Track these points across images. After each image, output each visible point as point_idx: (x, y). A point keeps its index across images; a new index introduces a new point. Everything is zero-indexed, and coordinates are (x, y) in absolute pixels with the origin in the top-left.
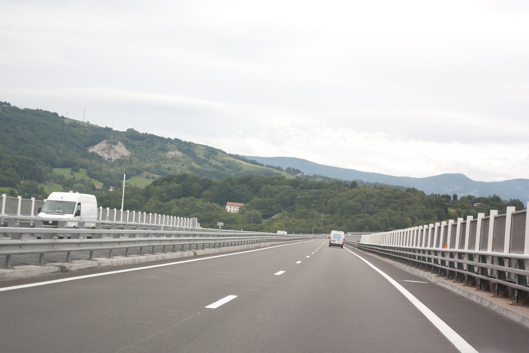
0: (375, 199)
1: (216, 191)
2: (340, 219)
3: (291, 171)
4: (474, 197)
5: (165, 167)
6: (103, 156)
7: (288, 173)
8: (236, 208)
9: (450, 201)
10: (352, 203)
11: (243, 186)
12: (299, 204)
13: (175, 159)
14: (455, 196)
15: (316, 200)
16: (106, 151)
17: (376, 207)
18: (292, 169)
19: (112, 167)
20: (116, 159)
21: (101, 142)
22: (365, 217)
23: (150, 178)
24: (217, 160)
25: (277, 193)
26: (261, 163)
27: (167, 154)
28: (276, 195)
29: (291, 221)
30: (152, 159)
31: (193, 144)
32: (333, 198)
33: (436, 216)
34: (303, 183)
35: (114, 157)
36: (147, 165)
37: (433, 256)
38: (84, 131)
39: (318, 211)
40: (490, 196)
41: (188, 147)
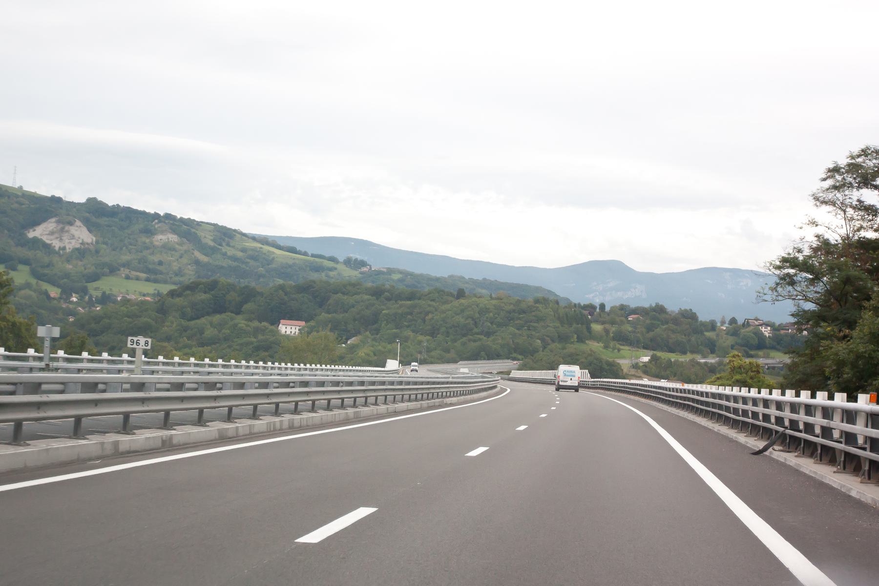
0: (491, 314)
1: (263, 304)
3: (352, 262)
4: (629, 306)
5: (153, 260)
6: (52, 243)
7: (347, 267)
8: (293, 328)
9: (595, 313)
10: (460, 319)
11: (303, 297)
12: (385, 322)
13: (167, 248)
14: (602, 306)
15: (409, 316)
16: (57, 235)
18: (353, 261)
19: (68, 261)
20: (73, 249)
21: (47, 220)
22: (480, 339)
23: (132, 279)
27: (154, 239)
28: (352, 309)
29: (380, 347)
32: (433, 313)
33: (575, 336)
34: (388, 291)
35: (70, 245)
36: (125, 258)
37: (760, 409)
38: (17, 202)
39: (413, 331)
40: (651, 305)
41: (188, 228)
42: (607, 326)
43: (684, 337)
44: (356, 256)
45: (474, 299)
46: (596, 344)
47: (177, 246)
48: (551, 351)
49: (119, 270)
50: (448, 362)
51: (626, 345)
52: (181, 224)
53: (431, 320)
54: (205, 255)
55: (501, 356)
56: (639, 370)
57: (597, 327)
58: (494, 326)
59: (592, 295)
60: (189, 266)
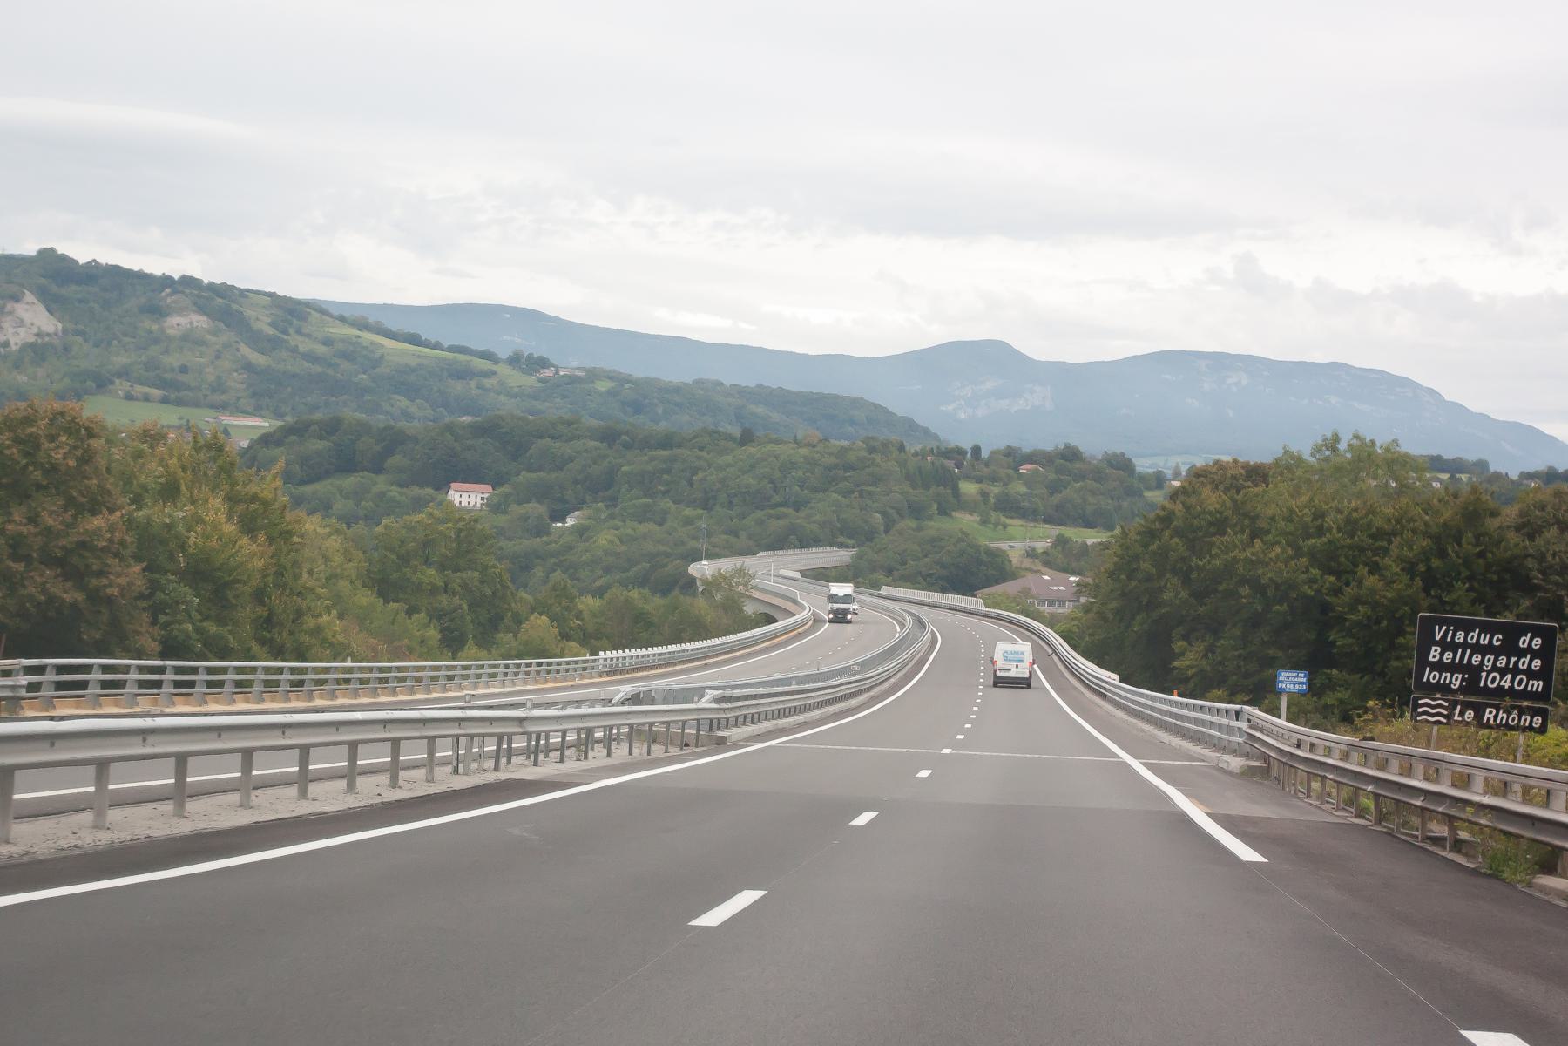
0: (800, 473)
8: (473, 496)
10: (749, 480)
13: (190, 339)
14: (976, 450)
15: (665, 476)
17: (806, 492)
22: (785, 516)
24: (308, 336)
25: (571, 460)
26: (433, 341)
30: (127, 339)
33: (935, 506)
34: (627, 433)
36: (120, 360)
42: (984, 486)
43: (1110, 502)
44: (531, 346)
45: (770, 447)
46: (968, 517)
47: (209, 337)
48: (900, 533)
49: (112, 383)
51: (1018, 517)
52: (213, 295)
53: (703, 480)
54: (262, 352)
56: (1036, 561)
57: (969, 488)
58: (806, 492)
59: (950, 408)
60: (235, 374)
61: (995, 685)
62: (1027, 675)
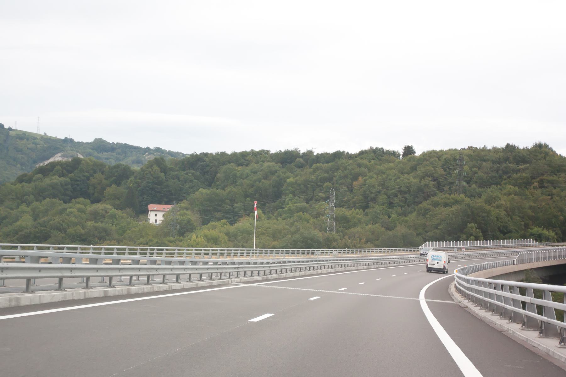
2: (387, 217)
8: (159, 214)
10: (412, 180)
11: (187, 174)
21: (54, 156)
31: (181, 155)
38: (33, 143)
50: (392, 244)
55: (510, 232)
61: (428, 271)
62: (442, 267)
